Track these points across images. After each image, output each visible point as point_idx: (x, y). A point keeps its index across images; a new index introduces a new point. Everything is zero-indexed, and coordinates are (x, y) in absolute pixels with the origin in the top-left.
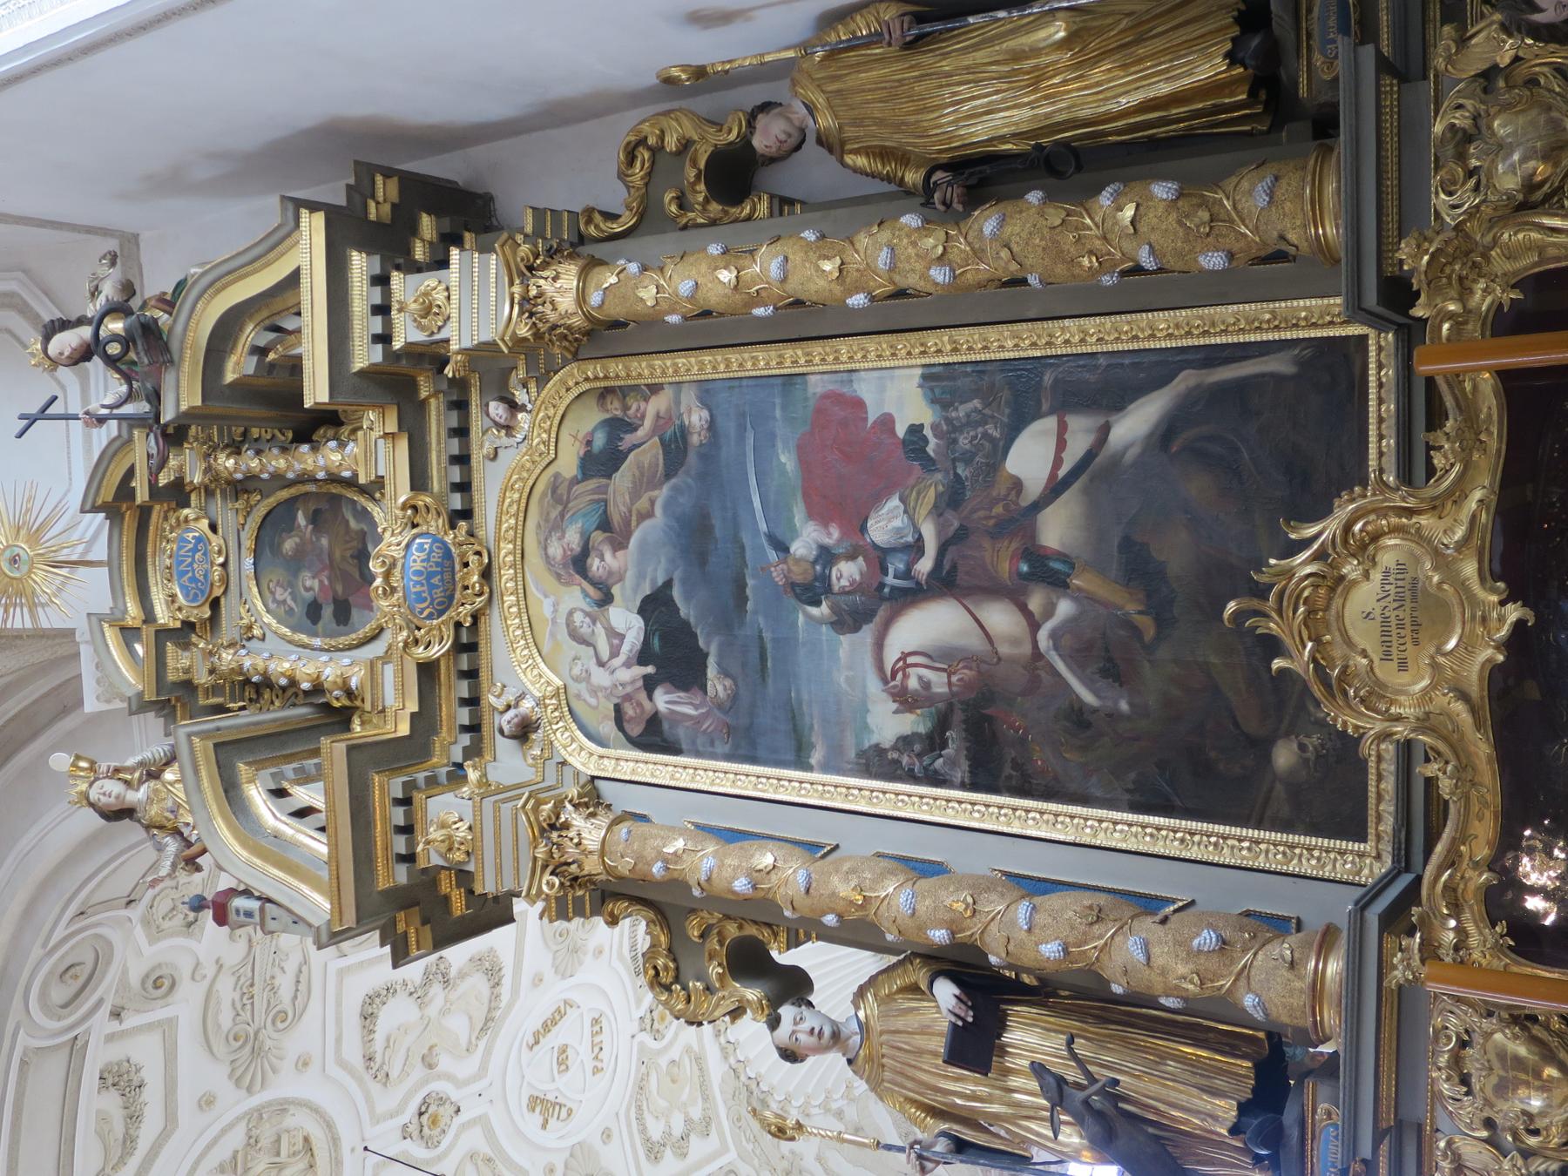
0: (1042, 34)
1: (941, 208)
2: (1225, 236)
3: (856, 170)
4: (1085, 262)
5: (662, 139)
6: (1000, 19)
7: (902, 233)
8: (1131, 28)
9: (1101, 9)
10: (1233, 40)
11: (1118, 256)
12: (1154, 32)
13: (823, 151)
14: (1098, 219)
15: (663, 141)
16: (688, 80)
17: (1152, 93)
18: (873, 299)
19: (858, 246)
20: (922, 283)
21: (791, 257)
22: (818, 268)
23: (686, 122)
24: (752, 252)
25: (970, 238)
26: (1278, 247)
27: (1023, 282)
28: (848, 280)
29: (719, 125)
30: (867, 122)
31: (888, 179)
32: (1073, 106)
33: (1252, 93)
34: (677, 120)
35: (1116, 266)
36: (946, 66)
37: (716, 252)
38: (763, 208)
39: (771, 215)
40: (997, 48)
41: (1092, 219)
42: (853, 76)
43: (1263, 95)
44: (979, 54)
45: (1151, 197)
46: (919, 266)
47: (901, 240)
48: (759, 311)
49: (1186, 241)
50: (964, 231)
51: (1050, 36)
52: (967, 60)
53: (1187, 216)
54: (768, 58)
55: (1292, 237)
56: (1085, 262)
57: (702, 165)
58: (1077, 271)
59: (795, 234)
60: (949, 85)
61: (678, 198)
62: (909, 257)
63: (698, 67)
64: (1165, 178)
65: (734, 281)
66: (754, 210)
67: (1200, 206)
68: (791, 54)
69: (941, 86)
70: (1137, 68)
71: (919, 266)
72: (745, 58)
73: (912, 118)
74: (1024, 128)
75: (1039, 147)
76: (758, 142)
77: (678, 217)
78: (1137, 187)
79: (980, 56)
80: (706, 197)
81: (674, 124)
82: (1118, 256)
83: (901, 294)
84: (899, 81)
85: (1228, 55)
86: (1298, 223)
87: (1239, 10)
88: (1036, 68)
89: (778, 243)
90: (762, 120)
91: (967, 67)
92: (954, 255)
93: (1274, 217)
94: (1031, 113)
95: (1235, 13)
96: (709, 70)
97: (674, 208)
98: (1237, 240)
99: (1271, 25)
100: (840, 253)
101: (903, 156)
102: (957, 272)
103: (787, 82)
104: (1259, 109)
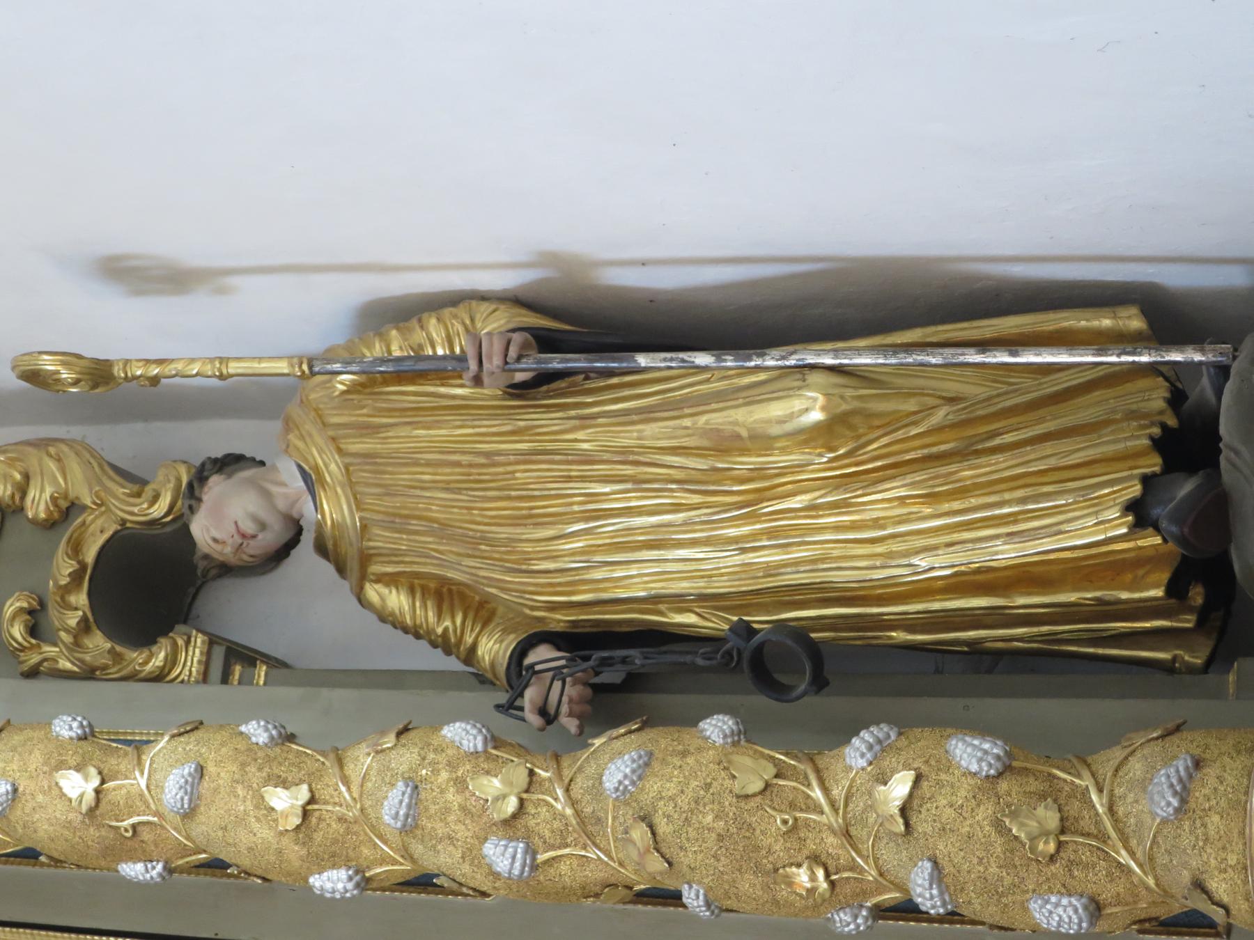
0: (776, 410)
1: (534, 719)
2: (1086, 866)
3: (386, 617)
4: (802, 877)
5: (23, 490)
6: (705, 369)
7: (442, 758)
8: (953, 426)
9: (899, 382)
10: (1146, 480)
11: (871, 874)
12: (997, 441)
13: (328, 568)
14: (838, 792)
15: (24, 494)
16: (76, 383)
17: (977, 557)
18: (365, 883)
19: (350, 769)
20: (466, 868)
21: (211, 768)
22: (260, 802)
23: (75, 468)
24: (139, 746)
25: (576, 791)
26: (1190, 904)
27: (674, 898)
28: (318, 837)
29: (136, 481)
30: (415, 525)
31: (445, 645)
32: (823, 560)
33: (1176, 589)
34: (59, 460)
35: (865, 894)
36: (586, 440)
37: (66, 733)
38: (192, 657)
39: (205, 678)
40: (687, 422)
41: (826, 790)
42: (403, 431)
43: (1197, 595)
44: (650, 429)
45: (947, 765)
46: (463, 832)
47: (436, 772)
48: (133, 870)
49: (1007, 865)
50: (567, 773)
51: (792, 416)
52: (627, 437)
53: (1014, 815)
54: (234, 367)
55: (1219, 887)
56: (802, 877)
57: (90, 555)
58: (783, 892)
59: (230, 724)
60: (583, 479)
61: (31, 612)
62: (447, 810)
63: (97, 361)
64: (983, 729)
65: (90, 796)
66: (172, 661)
67: (1043, 797)
68: (282, 367)
69: (569, 479)
70: (956, 505)
71: (463, 832)
72: (193, 360)
73: (504, 532)
74: (721, 586)
75: (746, 630)
76: (202, 529)
77: (23, 649)
78: (924, 739)
79: (653, 432)
80: (84, 619)
81: (52, 465)
82: (871, 874)
83: (423, 882)
84: (487, 454)
85: (1133, 507)
86: (1232, 859)
87: (1164, 426)
88: (758, 473)
89: (193, 737)
90: (216, 486)
91: (625, 451)
92: (538, 820)
93: (1186, 841)
94: (739, 559)
95: (1156, 431)
96: (118, 371)
97: (18, 631)
98: (1110, 877)
99: (1216, 465)
100: (311, 779)
101: (482, 605)
102: (541, 857)
103: (277, 425)
104: (1187, 622)
